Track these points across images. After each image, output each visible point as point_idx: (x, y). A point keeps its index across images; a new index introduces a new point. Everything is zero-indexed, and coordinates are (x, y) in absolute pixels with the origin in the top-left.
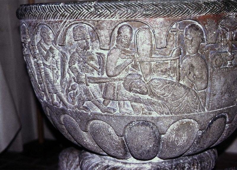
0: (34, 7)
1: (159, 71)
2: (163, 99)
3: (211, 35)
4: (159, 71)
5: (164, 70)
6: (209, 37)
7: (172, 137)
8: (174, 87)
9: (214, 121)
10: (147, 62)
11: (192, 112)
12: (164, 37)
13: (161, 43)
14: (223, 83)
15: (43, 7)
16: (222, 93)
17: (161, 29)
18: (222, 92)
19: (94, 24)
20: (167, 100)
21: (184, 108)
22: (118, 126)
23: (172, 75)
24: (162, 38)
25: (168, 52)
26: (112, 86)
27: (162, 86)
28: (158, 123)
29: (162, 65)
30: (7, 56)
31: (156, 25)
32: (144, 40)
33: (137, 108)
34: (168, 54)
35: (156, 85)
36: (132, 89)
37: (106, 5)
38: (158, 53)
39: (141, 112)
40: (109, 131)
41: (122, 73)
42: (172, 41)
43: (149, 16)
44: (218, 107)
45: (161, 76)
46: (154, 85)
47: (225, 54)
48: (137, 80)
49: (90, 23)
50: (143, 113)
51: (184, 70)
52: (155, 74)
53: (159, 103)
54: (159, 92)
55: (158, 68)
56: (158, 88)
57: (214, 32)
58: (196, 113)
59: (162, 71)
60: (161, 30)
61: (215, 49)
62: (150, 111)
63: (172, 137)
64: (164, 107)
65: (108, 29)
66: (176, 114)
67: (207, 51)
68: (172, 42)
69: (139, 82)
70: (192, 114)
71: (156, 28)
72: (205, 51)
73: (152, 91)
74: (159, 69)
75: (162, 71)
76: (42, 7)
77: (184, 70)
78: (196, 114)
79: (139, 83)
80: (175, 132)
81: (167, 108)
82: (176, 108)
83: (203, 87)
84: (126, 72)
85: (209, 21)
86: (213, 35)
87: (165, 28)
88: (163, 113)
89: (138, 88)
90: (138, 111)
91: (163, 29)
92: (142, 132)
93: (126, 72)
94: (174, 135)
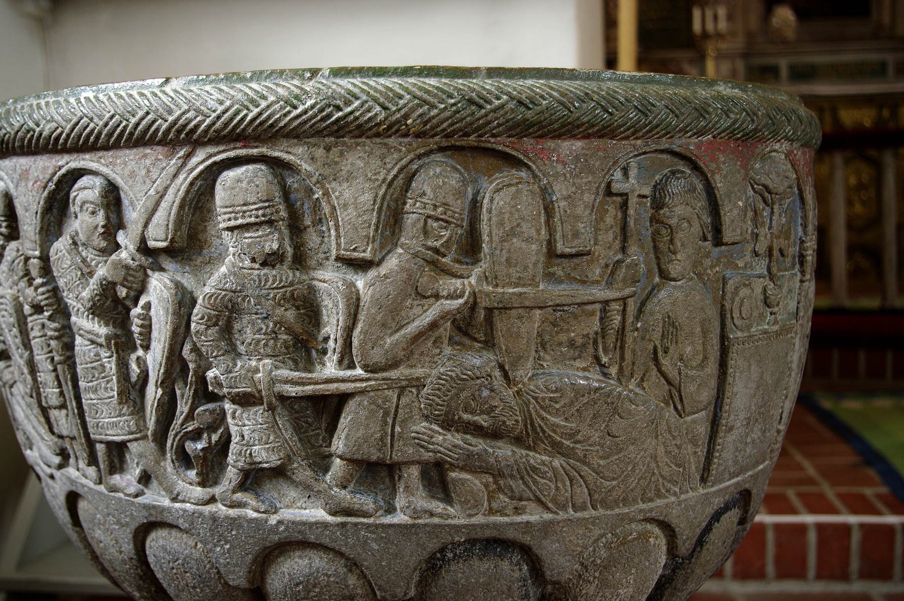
0: (47, 104)
1: (560, 344)
2: (566, 454)
3: (731, 210)
4: (560, 344)
5: (579, 341)
6: (727, 220)
7: (584, 592)
8: (613, 403)
9: (716, 523)
10: (520, 311)
11: (659, 495)
12: (587, 212)
13: (576, 235)
14: (754, 386)
15: (87, 99)
16: (749, 423)
17: (578, 181)
18: (749, 418)
19: (312, 159)
20: (585, 456)
21: (638, 483)
22: (389, 564)
23: (604, 360)
24: (578, 218)
25: (598, 271)
26: (378, 406)
27: (572, 403)
28: (545, 543)
29: (571, 320)
30: (190, 568)
31: (559, 167)
32: (515, 224)
33: (471, 492)
34: (595, 278)
35: (551, 399)
36: (456, 417)
37: (364, 83)
38: (560, 273)
39: (486, 504)
40: (347, 586)
41: (422, 354)
42: (612, 227)
43: (536, 128)
44: (734, 473)
45: (568, 363)
46: (544, 399)
47: (761, 283)
48: (478, 381)
49: (294, 155)
50: (491, 509)
51: (650, 340)
52: (548, 357)
53: (554, 470)
54: (562, 423)
55: (557, 333)
56: (557, 410)
57: (740, 203)
58: (673, 499)
59: (572, 344)
60: (574, 184)
61: (737, 265)
62: (521, 499)
63: (584, 592)
64: (571, 481)
65: (370, 179)
66: (612, 508)
67: (717, 268)
68: (611, 232)
69: (485, 387)
70: (659, 502)
71: (556, 175)
72: (709, 271)
73: (532, 424)
74: (563, 337)
75: (572, 344)
76: (83, 100)
77: (650, 340)
78: (673, 503)
79: (486, 393)
80: (597, 574)
81: (581, 486)
82: (614, 483)
83: (702, 401)
84: (438, 351)
85: (724, 163)
86: (736, 212)
87: (590, 179)
88: (564, 507)
89: (482, 412)
90: (476, 501)
91: (584, 180)
92: (481, 580)
93: (438, 351)
94: (593, 588)
